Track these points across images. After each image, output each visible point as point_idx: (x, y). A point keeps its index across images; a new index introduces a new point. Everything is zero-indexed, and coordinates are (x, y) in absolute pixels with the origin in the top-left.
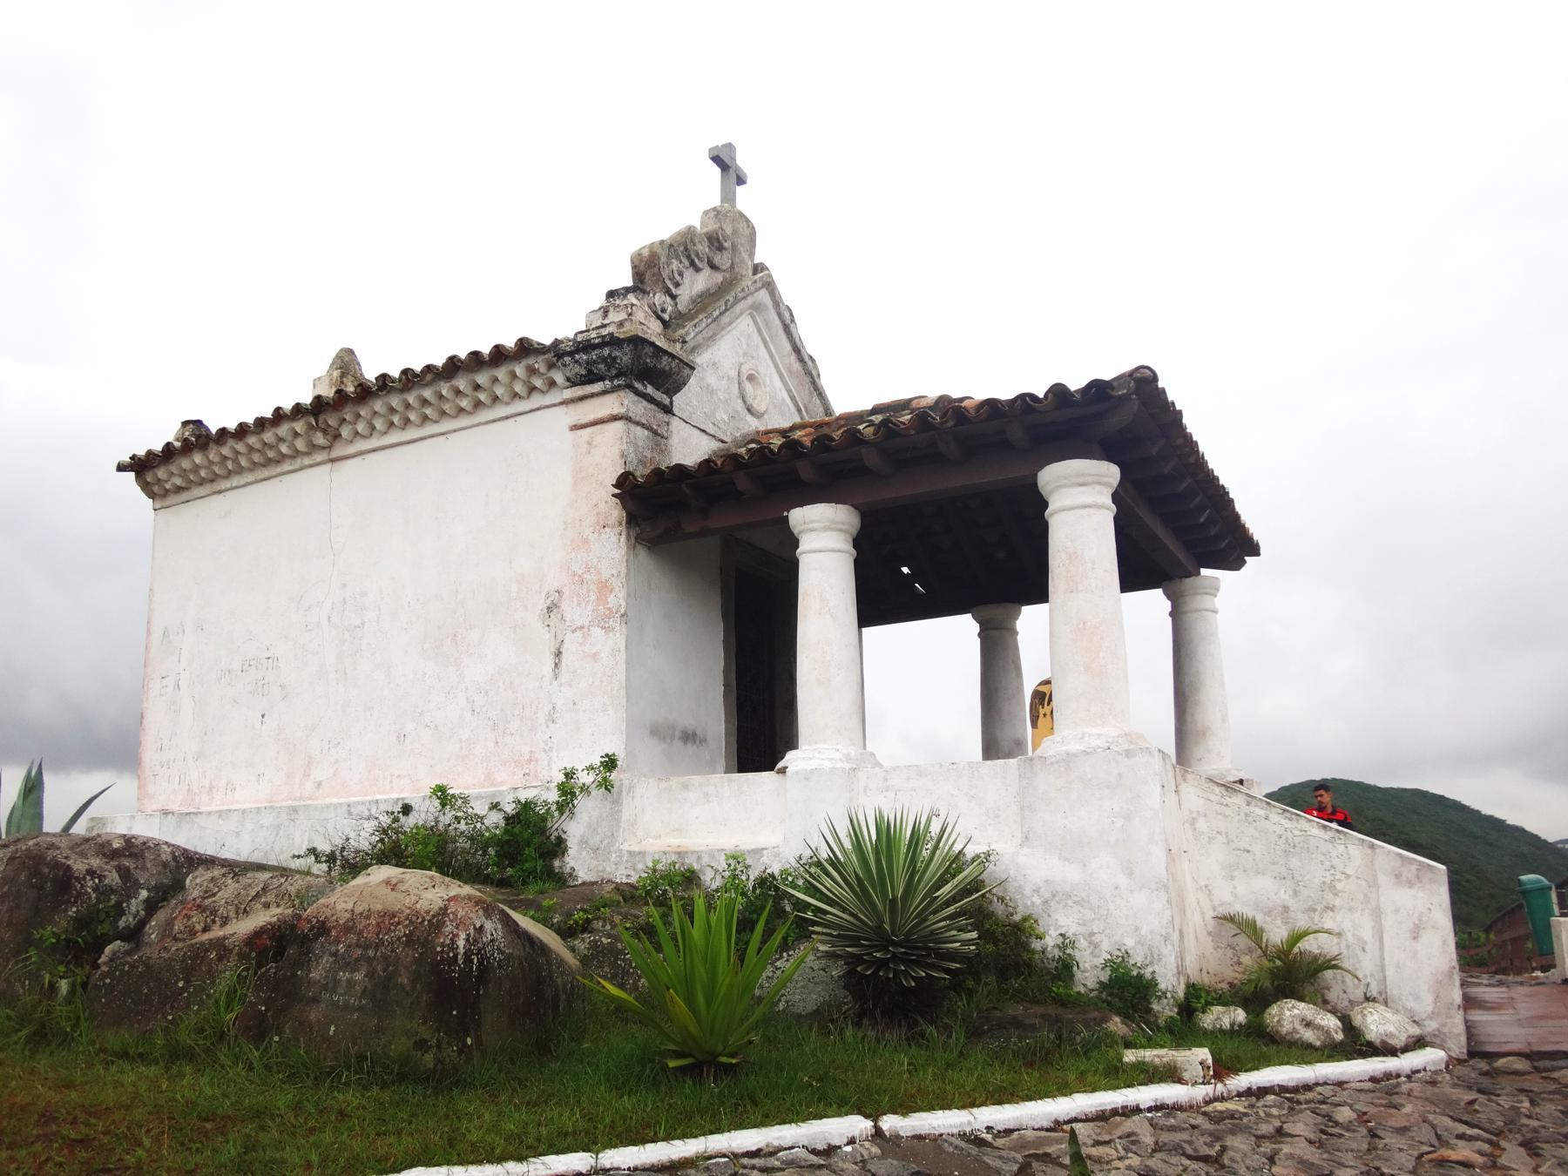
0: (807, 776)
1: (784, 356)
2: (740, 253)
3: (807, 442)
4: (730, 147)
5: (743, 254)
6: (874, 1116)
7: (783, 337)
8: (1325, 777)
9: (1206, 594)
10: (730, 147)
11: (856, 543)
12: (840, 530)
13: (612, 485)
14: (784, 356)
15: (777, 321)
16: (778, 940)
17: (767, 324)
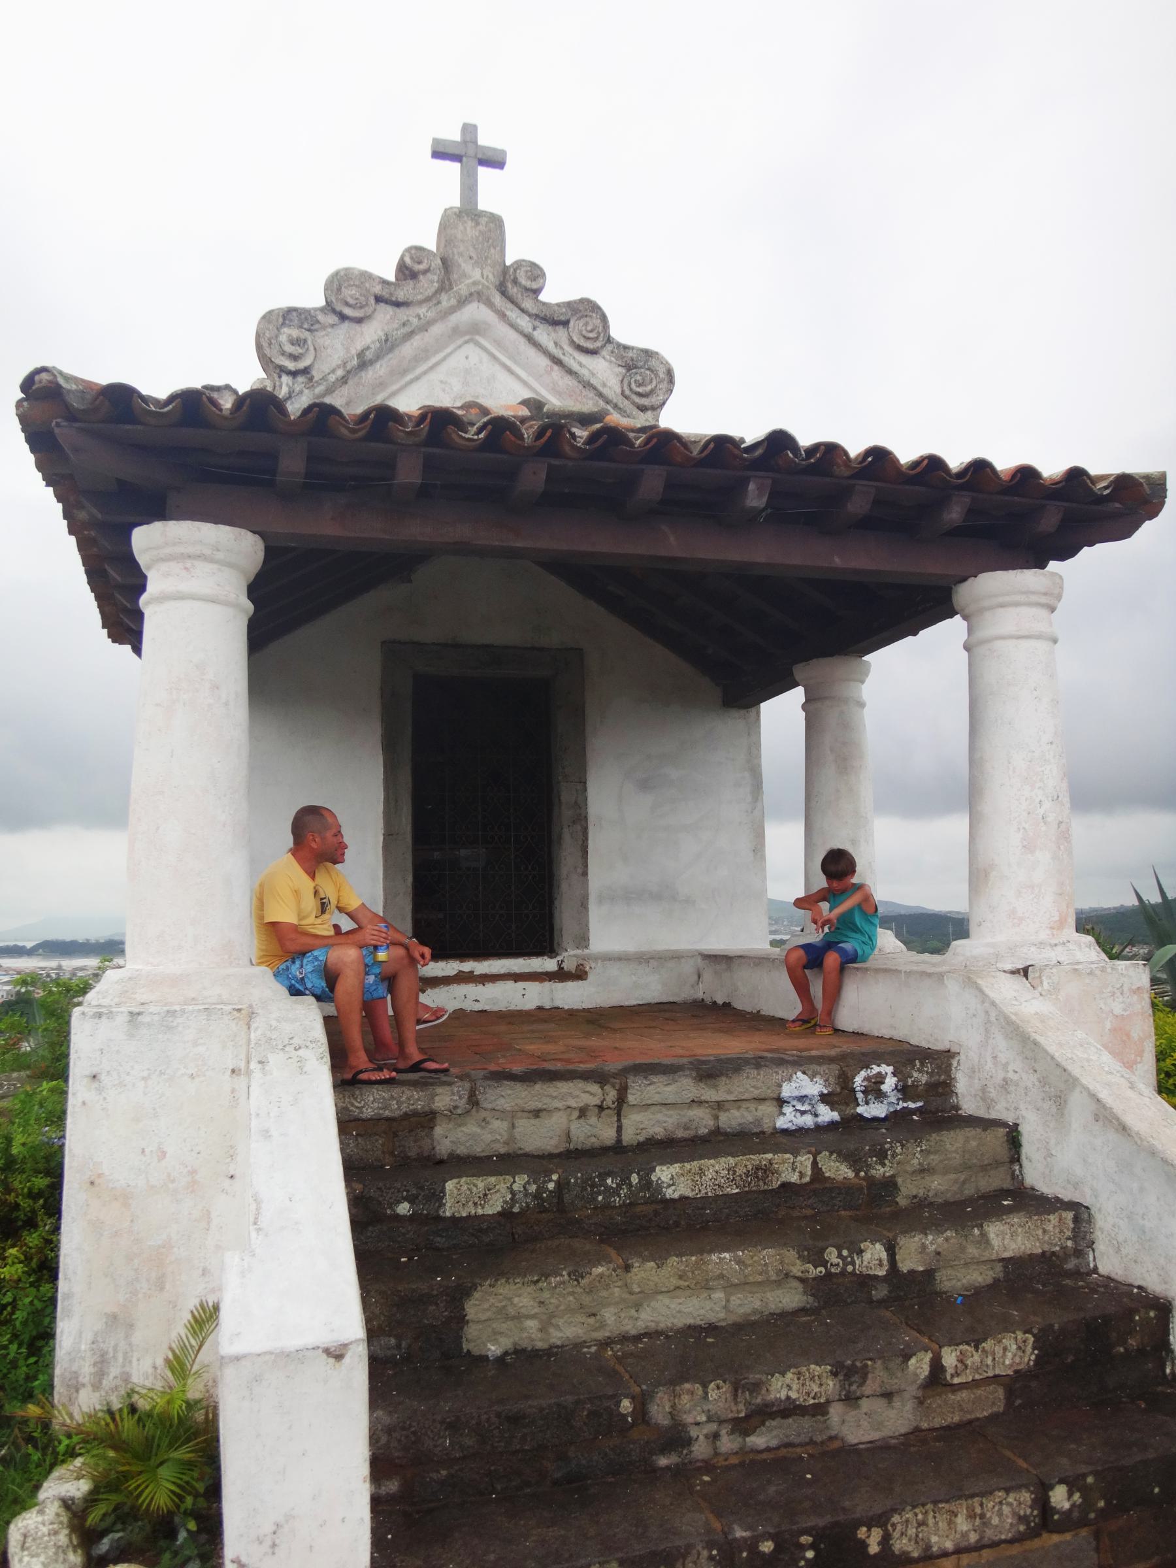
0: (1053, 574)
1: (541, 376)
2: (459, 266)
3: (294, 408)
4: (436, 142)
5: (463, 265)
6: (870, 1179)
7: (531, 352)
8: (24, 440)
9: (1002, 606)
10: (436, 142)
11: (255, 590)
12: (230, 565)
13: (137, 650)
14: (541, 376)
15: (512, 335)
16: (710, 1051)
17: (498, 343)
